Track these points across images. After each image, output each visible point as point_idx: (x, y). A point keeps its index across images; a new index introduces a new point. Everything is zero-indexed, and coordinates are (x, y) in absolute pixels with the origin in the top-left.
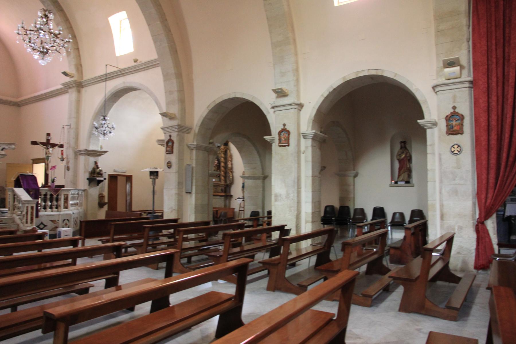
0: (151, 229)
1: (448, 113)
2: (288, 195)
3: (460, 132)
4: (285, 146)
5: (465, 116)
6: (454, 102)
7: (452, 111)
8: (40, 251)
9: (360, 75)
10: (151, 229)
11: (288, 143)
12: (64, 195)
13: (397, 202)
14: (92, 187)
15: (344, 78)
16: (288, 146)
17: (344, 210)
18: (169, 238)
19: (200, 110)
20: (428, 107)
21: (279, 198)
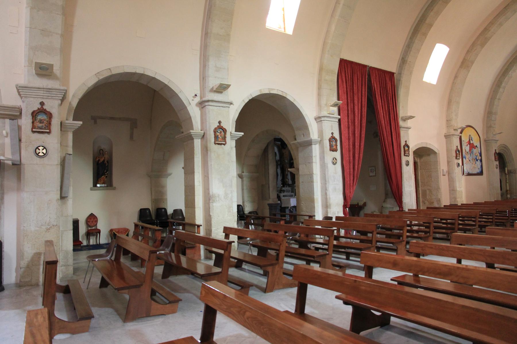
0: (511, 220)
1: (36, 109)
2: (226, 195)
3: (336, 150)
4: (221, 144)
5: (53, 115)
6: (332, 130)
7: (39, 106)
8: (308, 262)
9: (272, 92)
10: (511, 220)
11: (50, 129)
13: (293, 202)
15: (260, 90)
16: (49, 133)
17: (161, 212)
18: (362, 235)
19: (80, 80)
20: (312, 129)
21: (217, 199)
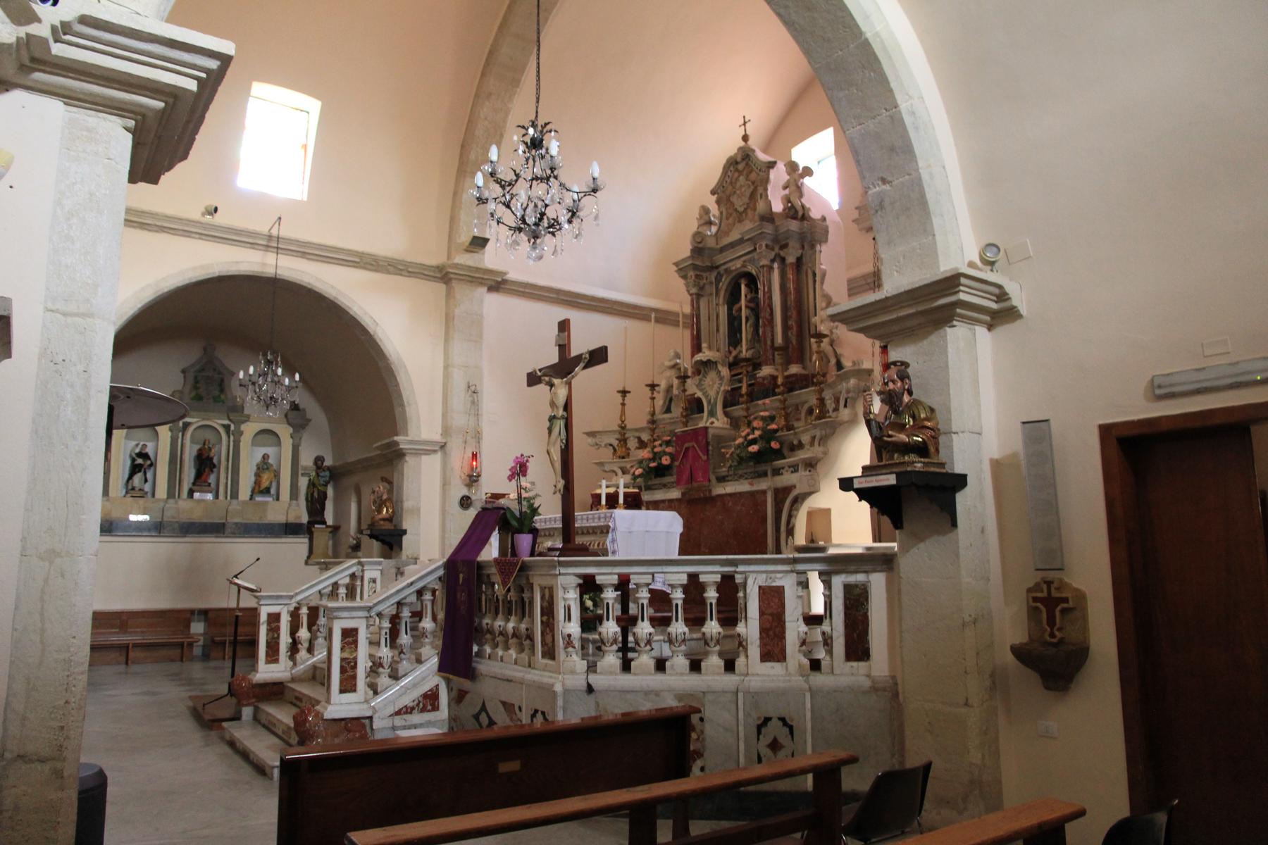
12: (543, 589)
14: (919, 538)
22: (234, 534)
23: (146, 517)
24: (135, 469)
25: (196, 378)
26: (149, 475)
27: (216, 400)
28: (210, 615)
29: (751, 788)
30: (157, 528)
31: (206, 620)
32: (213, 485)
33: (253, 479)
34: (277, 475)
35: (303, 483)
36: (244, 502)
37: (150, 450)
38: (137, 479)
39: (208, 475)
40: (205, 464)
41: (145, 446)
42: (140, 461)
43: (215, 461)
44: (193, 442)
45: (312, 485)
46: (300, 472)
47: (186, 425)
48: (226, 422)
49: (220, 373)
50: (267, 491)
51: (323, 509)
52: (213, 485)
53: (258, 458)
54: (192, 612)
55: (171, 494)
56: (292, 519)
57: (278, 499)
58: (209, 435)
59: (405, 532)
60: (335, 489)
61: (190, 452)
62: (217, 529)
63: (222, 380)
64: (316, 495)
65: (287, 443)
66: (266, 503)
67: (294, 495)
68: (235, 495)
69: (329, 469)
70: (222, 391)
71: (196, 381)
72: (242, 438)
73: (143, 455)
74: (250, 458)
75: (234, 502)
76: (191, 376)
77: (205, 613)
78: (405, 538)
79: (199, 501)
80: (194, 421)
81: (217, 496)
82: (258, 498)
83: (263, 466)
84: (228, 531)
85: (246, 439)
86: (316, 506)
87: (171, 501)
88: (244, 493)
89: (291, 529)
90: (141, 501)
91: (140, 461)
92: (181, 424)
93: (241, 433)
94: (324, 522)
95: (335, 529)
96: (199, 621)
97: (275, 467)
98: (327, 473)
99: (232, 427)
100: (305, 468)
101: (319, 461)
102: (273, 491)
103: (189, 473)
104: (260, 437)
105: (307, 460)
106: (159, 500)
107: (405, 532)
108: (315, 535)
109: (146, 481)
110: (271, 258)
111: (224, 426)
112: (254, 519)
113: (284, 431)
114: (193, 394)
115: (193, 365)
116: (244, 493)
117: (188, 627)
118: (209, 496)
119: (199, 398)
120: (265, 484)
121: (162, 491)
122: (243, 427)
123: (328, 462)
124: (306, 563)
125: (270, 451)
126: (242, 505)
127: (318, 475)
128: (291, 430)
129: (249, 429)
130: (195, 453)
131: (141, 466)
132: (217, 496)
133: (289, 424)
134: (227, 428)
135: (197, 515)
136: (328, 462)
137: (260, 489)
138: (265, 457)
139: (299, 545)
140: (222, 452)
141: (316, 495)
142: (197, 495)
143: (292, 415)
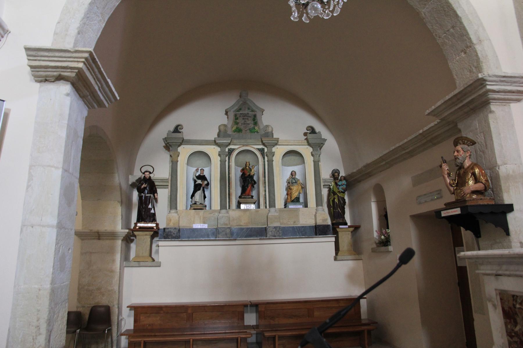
22: (275, 237)
23: (206, 226)
24: (197, 187)
25: (236, 115)
26: (207, 193)
27: (252, 131)
28: (261, 308)
29: (237, 331)
30: (216, 234)
31: (257, 311)
32: (255, 198)
33: (285, 193)
34: (304, 187)
35: (325, 192)
36: (280, 210)
37: (206, 174)
38: (199, 194)
39: (251, 190)
40: (248, 181)
41: (202, 170)
42: (199, 182)
43: (255, 178)
44: (237, 164)
45: (331, 192)
46: (322, 184)
47: (231, 151)
48: (261, 147)
49: (253, 111)
50: (296, 200)
51: (344, 213)
52: (255, 198)
53: (288, 175)
54: (245, 306)
55: (223, 206)
56: (320, 222)
57: (306, 206)
58: (248, 158)
59: (510, 208)
60: (349, 196)
61: (235, 174)
62: (260, 233)
63: (255, 116)
64: (336, 200)
65: (309, 160)
66: (297, 210)
67: (319, 203)
68: (272, 204)
69: (345, 178)
70: (256, 124)
71: (236, 118)
72: (274, 158)
73: (202, 177)
74: (282, 175)
75: (272, 209)
76: (231, 114)
77: (256, 306)
78: (510, 217)
79: (245, 210)
80: (237, 148)
81: (259, 207)
82: (291, 206)
83: (292, 181)
84: (269, 234)
85: (277, 159)
86: (336, 211)
87: (224, 211)
88: (280, 203)
89: (319, 230)
90: (201, 212)
91: (199, 182)
92: (227, 150)
93: (273, 154)
94: (346, 224)
95: (356, 228)
96: (251, 312)
97: (301, 181)
98: (344, 182)
99: (266, 150)
100: (325, 181)
101: (335, 174)
102: (302, 200)
103: (236, 190)
104: (285, 159)
105: (326, 174)
106: (215, 211)
107: (510, 208)
108: (340, 234)
109: (205, 197)
110: (116, 324)
111: (259, 150)
112: (289, 223)
113: (306, 151)
114: (234, 128)
115: (233, 106)
116: (280, 203)
117: (242, 318)
118: (253, 207)
119: (238, 130)
120: (295, 195)
121: (216, 204)
122: (274, 149)
123: (342, 174)
124: (336, 259)
125: (297, 169)
126: (277, 214)
127: (336, 184)
128: (311, 149)
129: (279, 151)
130: (240, 174)
131: (200, 185)
132: (259, 207)
133: (309, 144)
134: (262, 151)
135: (245, 222)
136: (342, 174)
137: (292, 200)
138: (293, 174)
139: (327, 244)
140: (259, 170)
141: (336, 200)
142: (243, 206)
143: (310, 136)
